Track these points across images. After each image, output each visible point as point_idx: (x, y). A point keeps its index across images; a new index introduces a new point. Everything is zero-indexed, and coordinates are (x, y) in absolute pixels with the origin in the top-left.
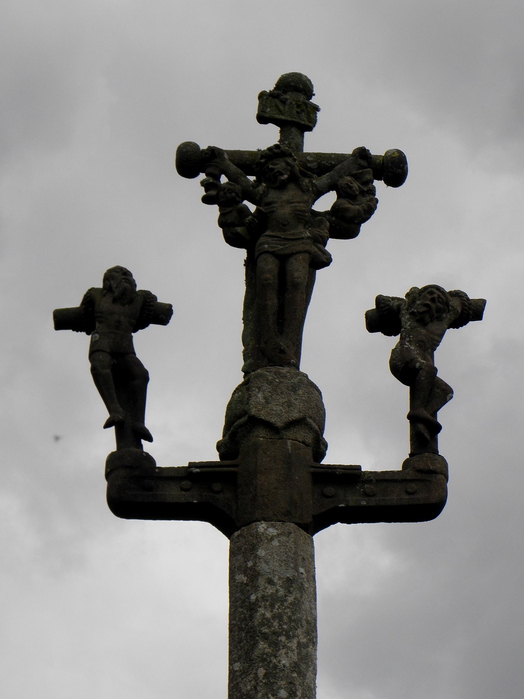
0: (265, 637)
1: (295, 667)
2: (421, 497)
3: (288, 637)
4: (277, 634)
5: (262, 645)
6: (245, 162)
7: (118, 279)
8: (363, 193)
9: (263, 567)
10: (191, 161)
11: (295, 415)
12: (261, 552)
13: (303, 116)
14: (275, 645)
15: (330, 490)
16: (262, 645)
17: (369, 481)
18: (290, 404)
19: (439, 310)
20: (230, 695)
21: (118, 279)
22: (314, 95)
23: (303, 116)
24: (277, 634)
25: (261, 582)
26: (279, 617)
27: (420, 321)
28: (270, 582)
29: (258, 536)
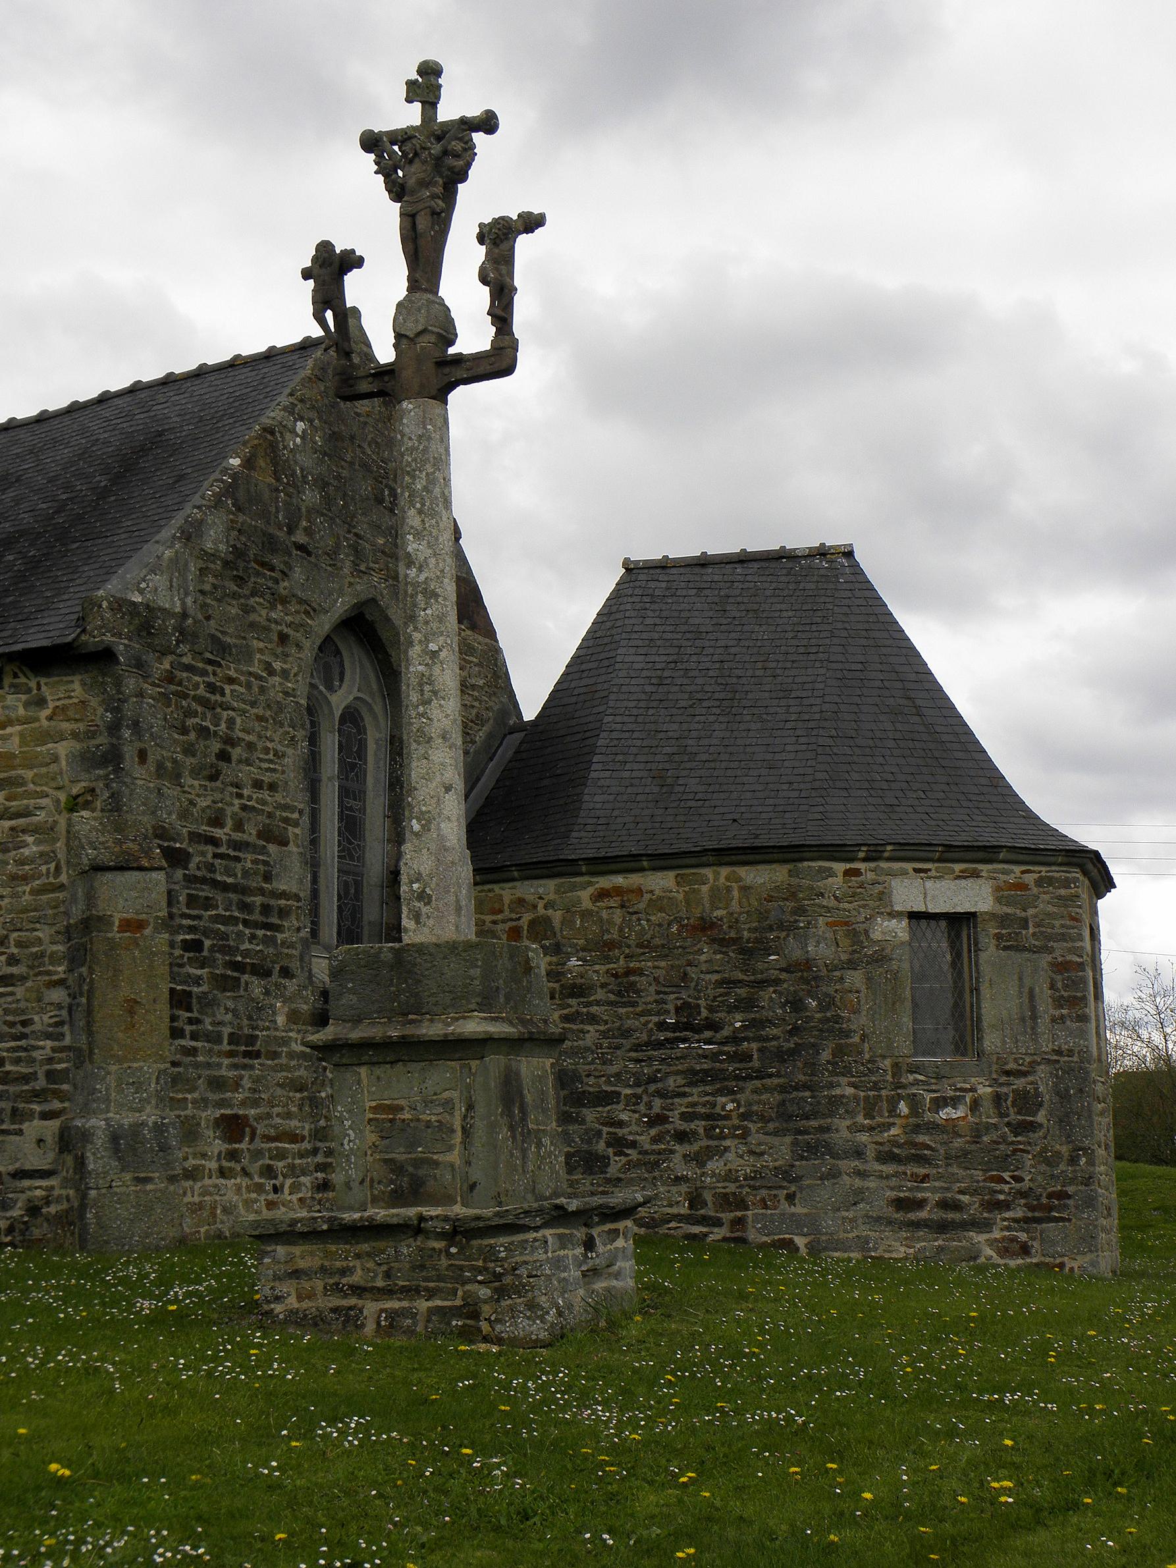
0: (408, 473)
1: (425, 488)
2: (504, 365)
3: (420, 471)
4: (414, 470)
5: (407, 478)
6: (403, 137)
7: (325, 248)
8: (465, 150)
9: (407, 430)
10: (371, 142)
11: (420, 328)
12: (405, 421)
13: (431, 95)
14: (414, 477)
15: (447, 370)
16: (407, 478)
17: (469, 360)
18: (417, 321)
19: (504, 234)
20: (12, 425)
21: (325, 248)
22: (306, 274)
23: (431, 95)
24: (414, 470)
25: (405, 439)
26: (415, 460)
27: (500, 237)
28: (410, 439)
29: (403, 410)
